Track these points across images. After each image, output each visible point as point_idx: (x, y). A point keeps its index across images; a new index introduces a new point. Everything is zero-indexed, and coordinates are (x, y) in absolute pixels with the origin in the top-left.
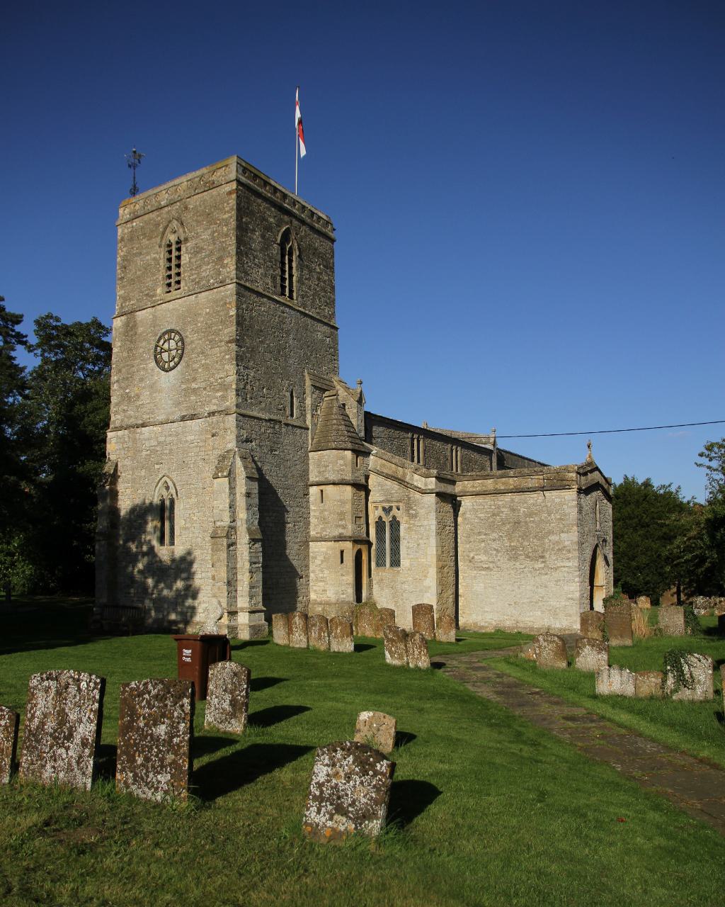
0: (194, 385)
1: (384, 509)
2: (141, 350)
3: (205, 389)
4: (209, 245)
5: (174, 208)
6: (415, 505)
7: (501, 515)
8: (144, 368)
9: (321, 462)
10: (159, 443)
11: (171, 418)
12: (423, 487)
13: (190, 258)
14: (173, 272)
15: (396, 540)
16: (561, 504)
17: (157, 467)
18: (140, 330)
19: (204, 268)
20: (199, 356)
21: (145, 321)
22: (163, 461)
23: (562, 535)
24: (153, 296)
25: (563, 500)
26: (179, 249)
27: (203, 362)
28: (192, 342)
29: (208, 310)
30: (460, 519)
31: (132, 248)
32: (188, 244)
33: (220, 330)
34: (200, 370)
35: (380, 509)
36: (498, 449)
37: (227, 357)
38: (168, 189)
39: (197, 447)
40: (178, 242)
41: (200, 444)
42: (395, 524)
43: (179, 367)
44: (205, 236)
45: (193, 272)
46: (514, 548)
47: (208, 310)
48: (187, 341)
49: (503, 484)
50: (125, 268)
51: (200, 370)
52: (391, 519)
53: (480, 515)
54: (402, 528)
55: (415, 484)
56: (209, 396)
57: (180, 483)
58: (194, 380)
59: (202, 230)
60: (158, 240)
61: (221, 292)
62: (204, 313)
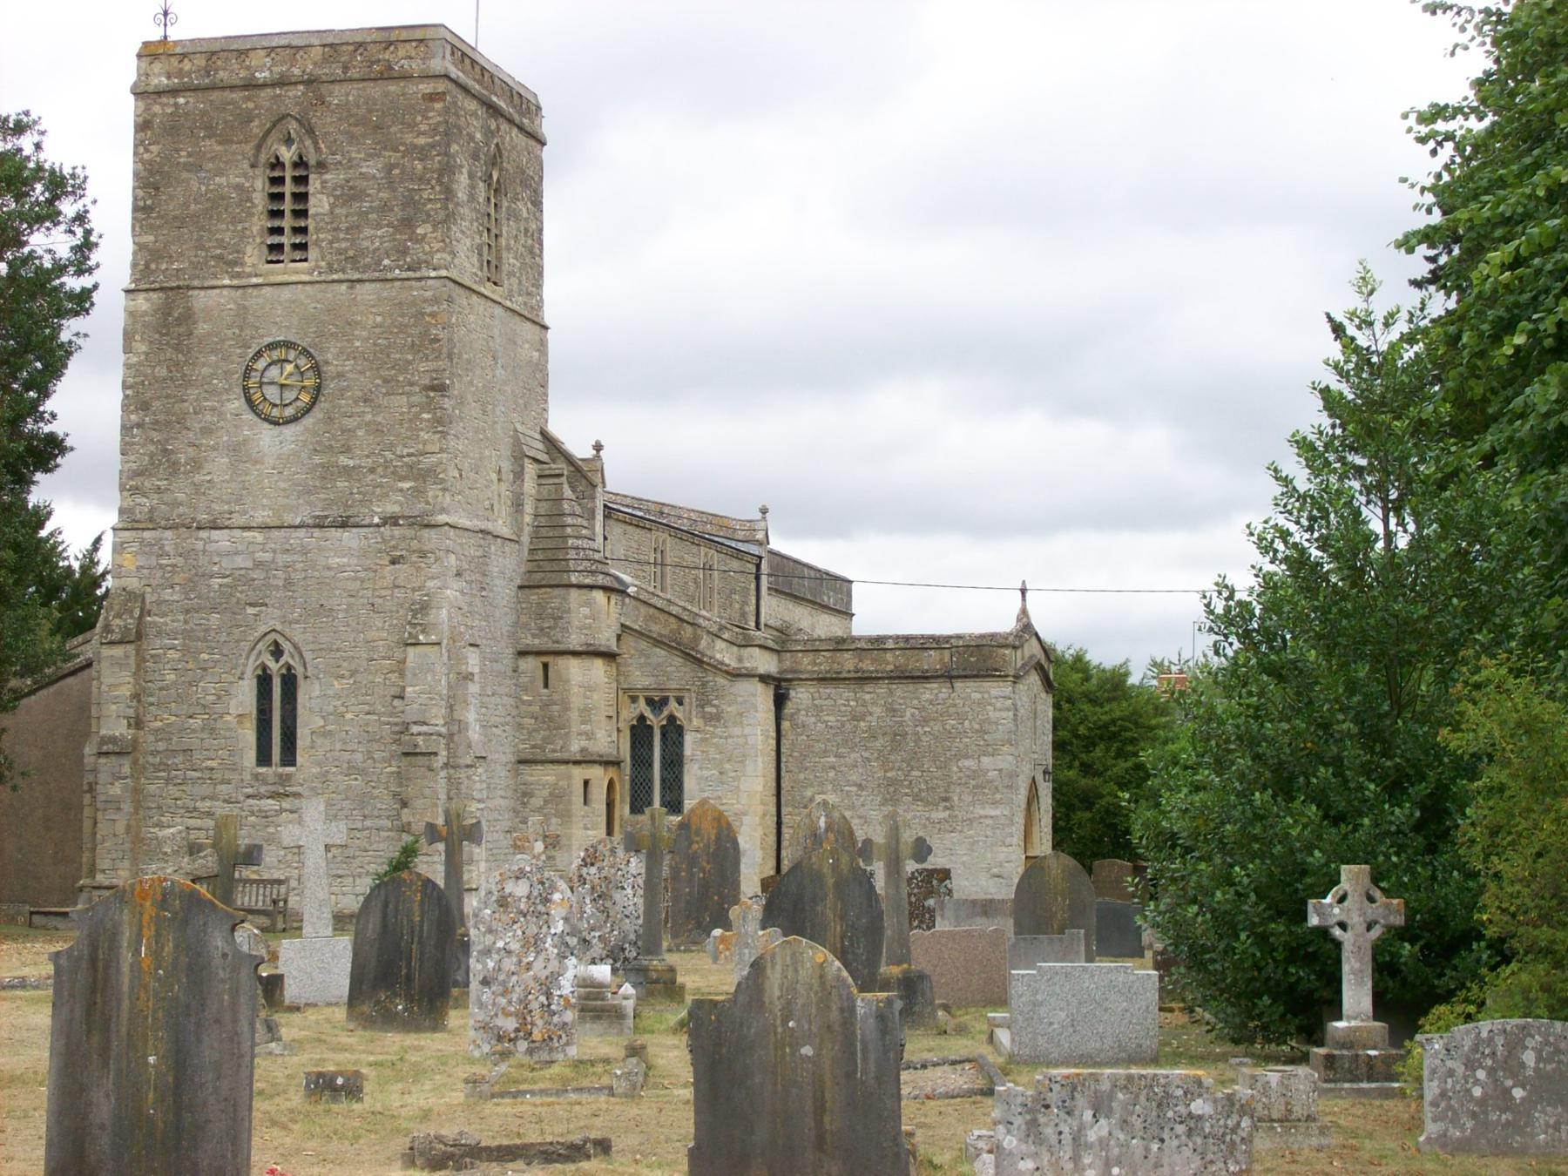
0: (344, 460)
1: (650, 702)
2: (206, 371)
3: (372, 470)
4: (379, 190)
5: (290, 94)
6: (717, 698)
7: (869, 718)
8: (213, 409)
9: (544, 609)
10: (259, 565)
11: (289, 519)
12: (734, 664)
13: (333, 206)
14: (287, 222)
15: (674, 764)
16: (982, 704)
17: (250, 610)
18: (202, 328)
19: (368, 232)
20: (357, 405)
21: (216, 313)
22: (267, 600)
23: (982, 759)
24: (235, 263)
25: (986, 696)
26: (302, 180)
27: (368, 417)
28: (340, 375)
29: (379, 319)
30: (785, 725)
31: (177, 151)
32: (328, 177)
33: (409, 362)
34: (360, 433)
35: (642, 702)
36: (771, 552)
37: (425, 416)
38: (273, 49)
39: (355, 579)
40: (300, 163)
41: (362, 575)
42: (674, 732)
43: (308, 421)
44: (372, 168)
45: (342, 236)
46: (892, 782)
47: (379, 319)
48: (329, 370)
49: (874, 660)
50: (157, 189)
51: (360, 433)
52: (665, 723)
53: (826, 718)
54: (689, 739)
55: (718, 656)
56: (381, 486)
57: (311, 647)
58: (347, 450)
59: (362, 156)
60: (249, 148)
61: (411, 288)
62: (370, 322)
